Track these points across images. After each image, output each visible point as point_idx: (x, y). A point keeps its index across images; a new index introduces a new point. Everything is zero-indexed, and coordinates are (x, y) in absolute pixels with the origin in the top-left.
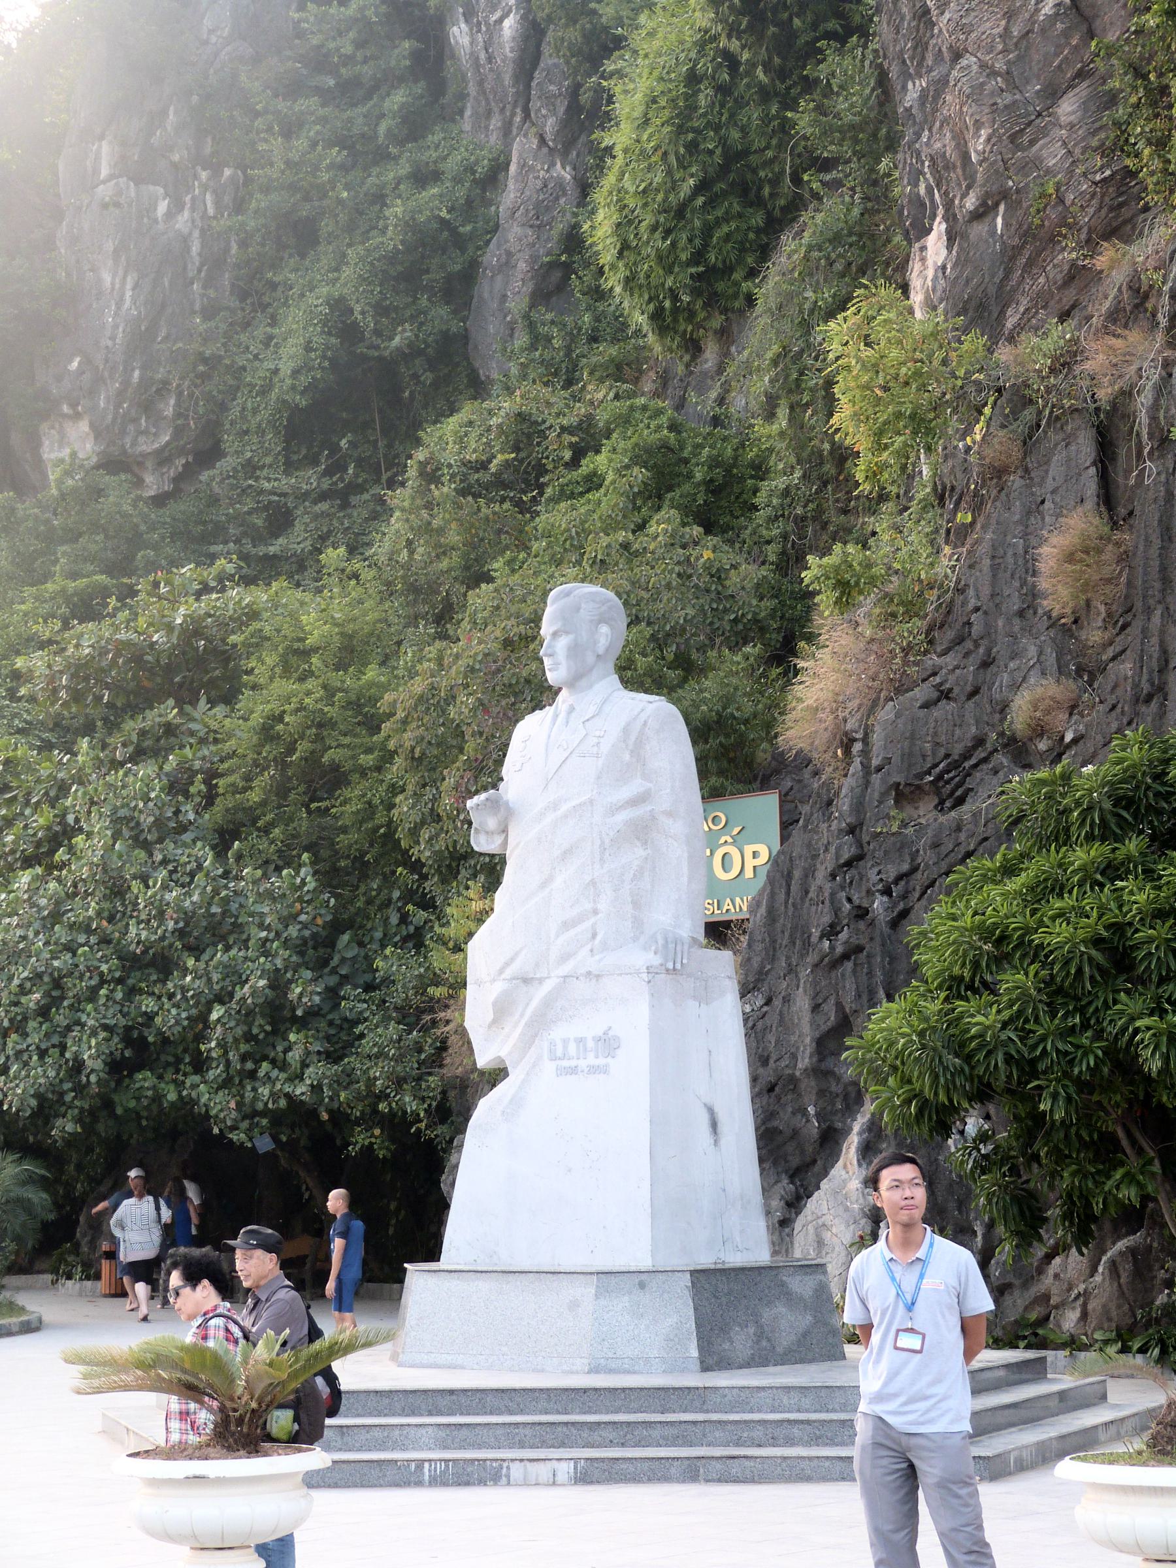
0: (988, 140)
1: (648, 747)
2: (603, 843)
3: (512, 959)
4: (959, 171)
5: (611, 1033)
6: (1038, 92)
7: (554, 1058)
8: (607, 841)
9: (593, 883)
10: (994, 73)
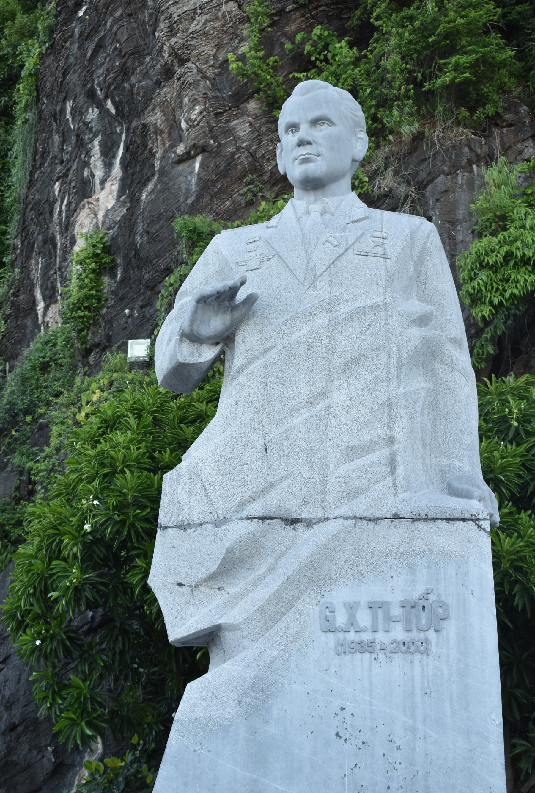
0: (201, 113)
1: (430, 264)
2: (400, 358)
3: (263, 492)
4: (165, 135)
5: (432, 597)
6: (230, 96)
7: (329, 628)
8: (405, 356)
9: (389, 403)
10: (205, 77)
